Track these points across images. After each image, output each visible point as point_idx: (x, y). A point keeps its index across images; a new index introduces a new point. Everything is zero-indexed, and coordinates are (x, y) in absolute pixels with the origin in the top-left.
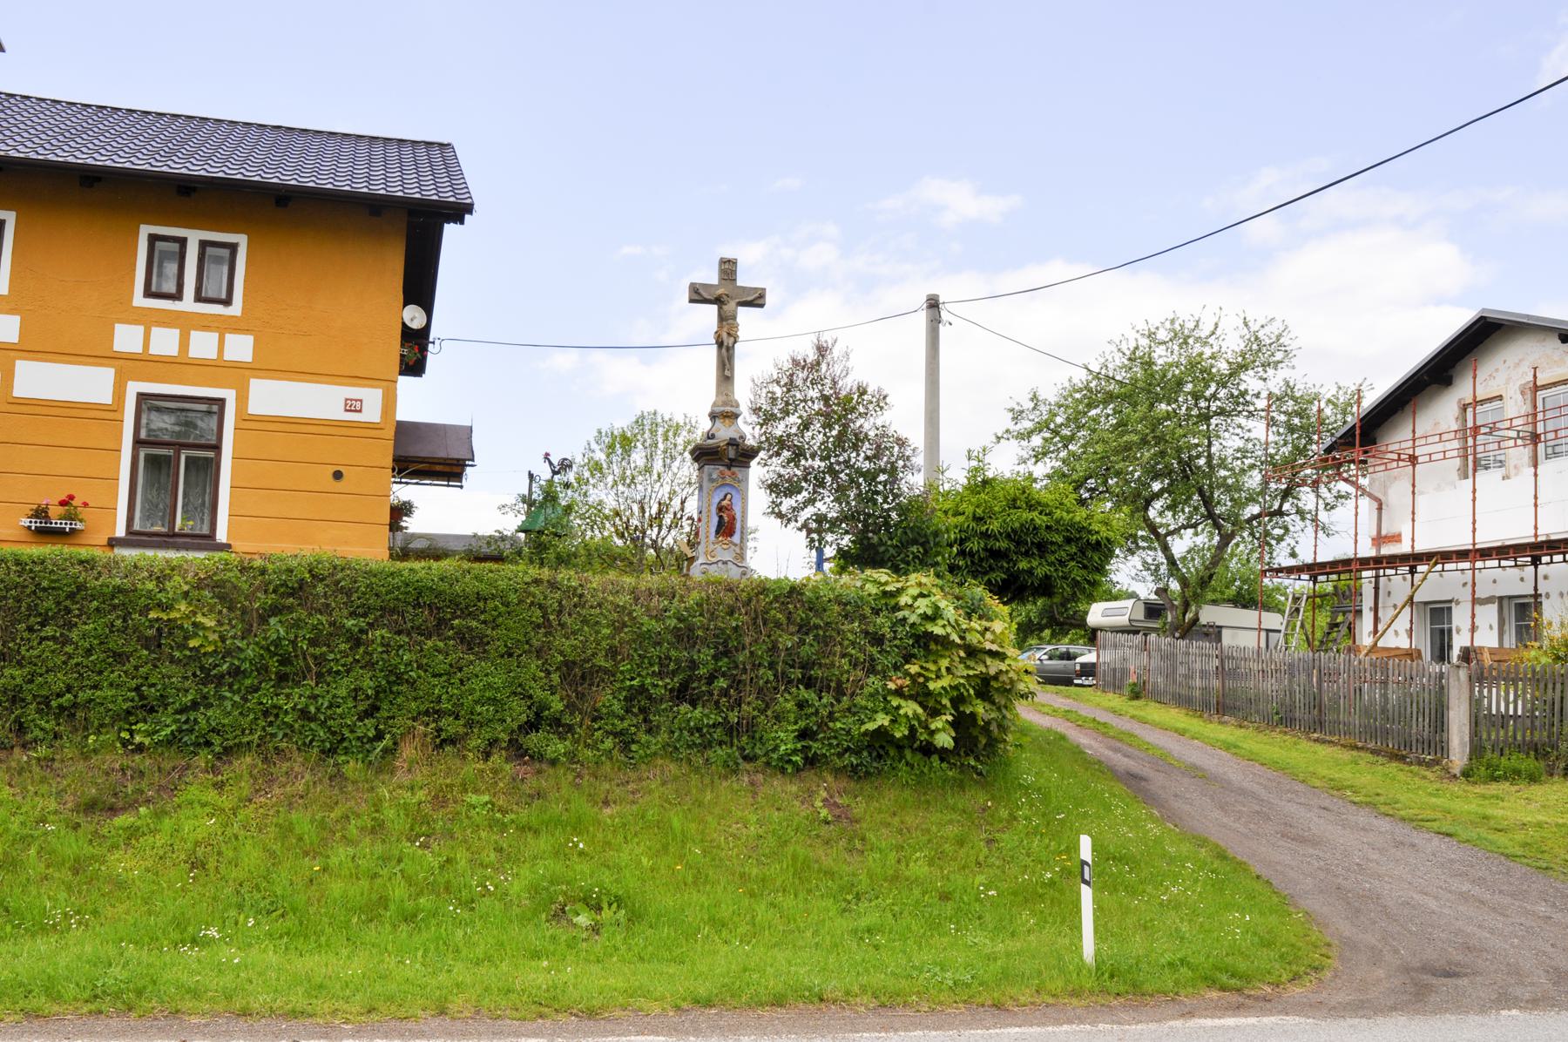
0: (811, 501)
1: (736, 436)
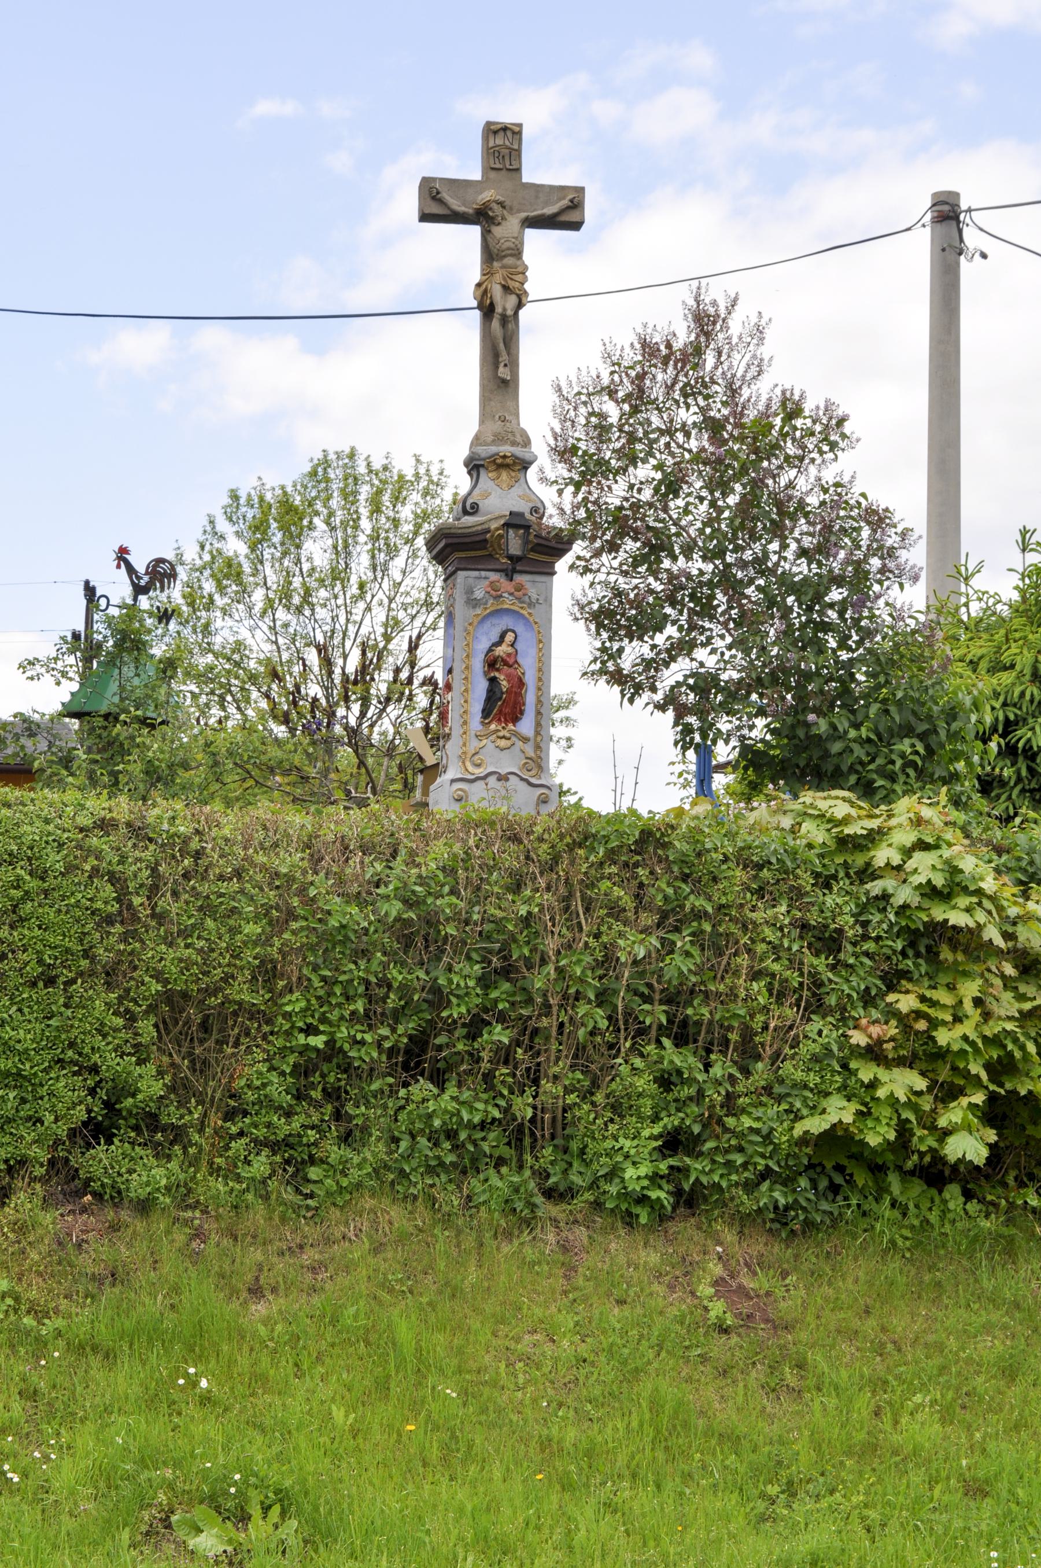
0: (683, 647)
1: (523, 507)
